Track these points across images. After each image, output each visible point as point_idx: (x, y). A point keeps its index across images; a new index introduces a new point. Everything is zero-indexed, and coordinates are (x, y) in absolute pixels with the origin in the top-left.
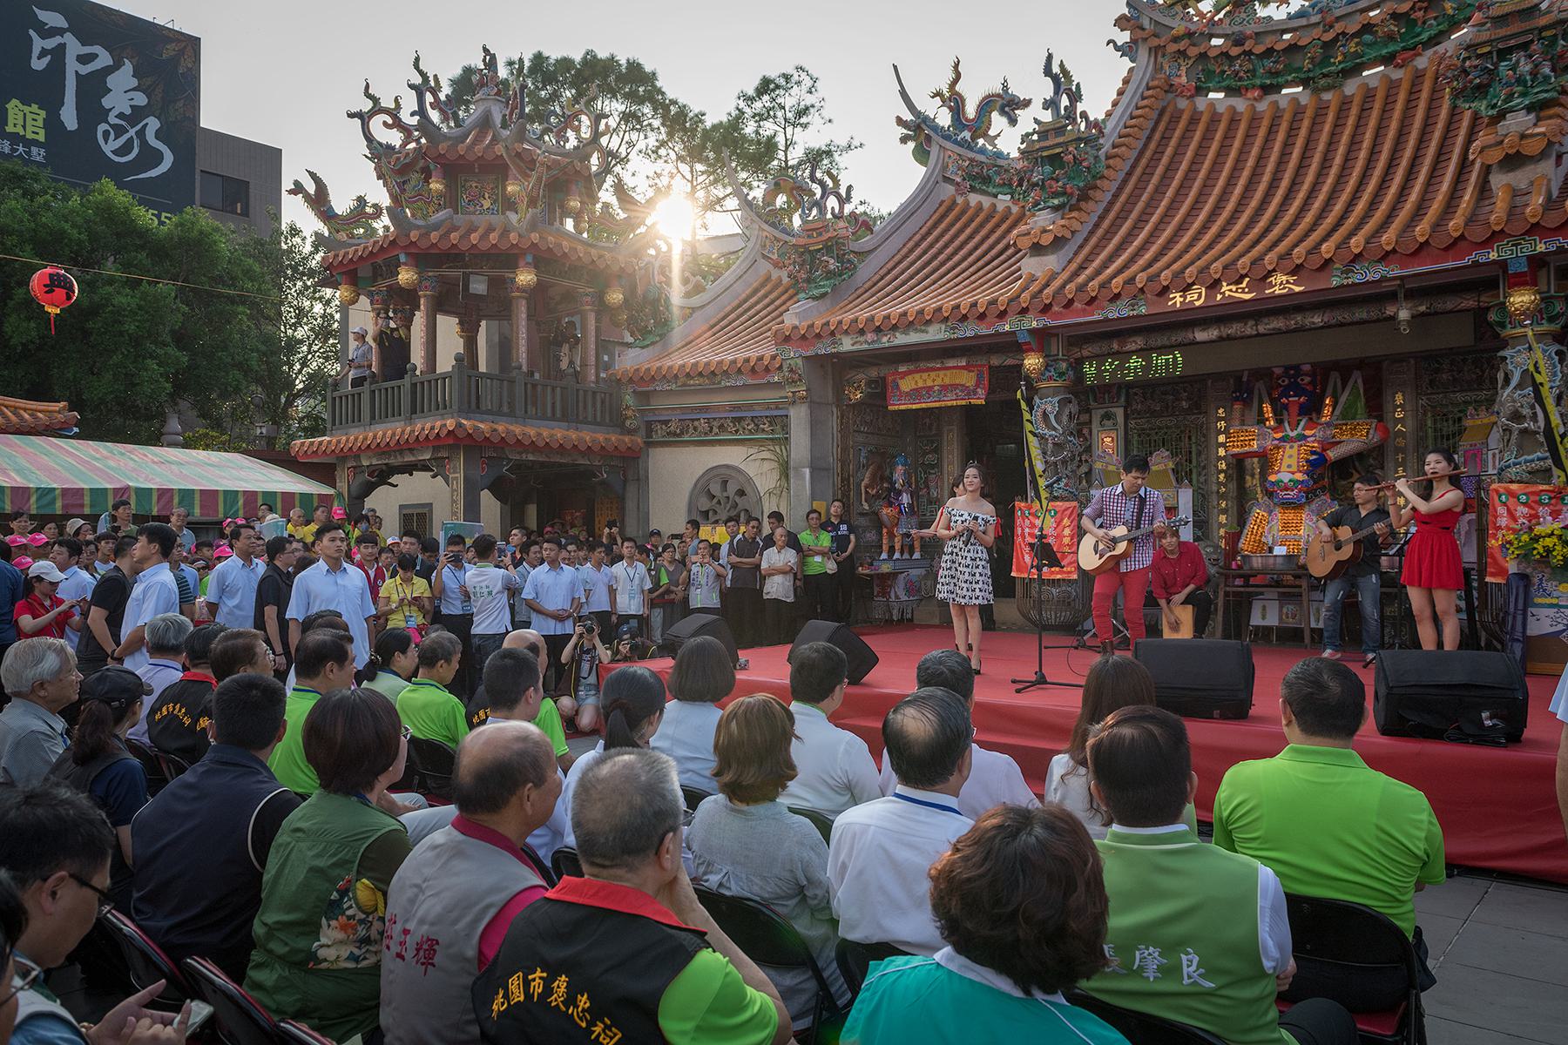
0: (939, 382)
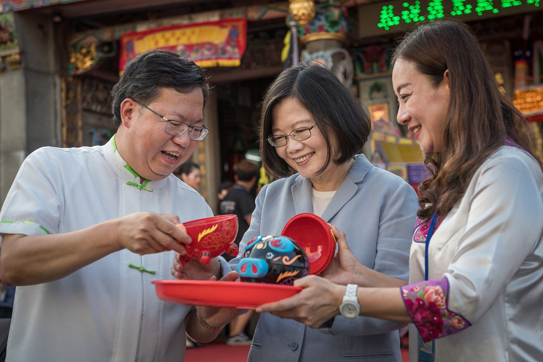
0: (184, 40)
